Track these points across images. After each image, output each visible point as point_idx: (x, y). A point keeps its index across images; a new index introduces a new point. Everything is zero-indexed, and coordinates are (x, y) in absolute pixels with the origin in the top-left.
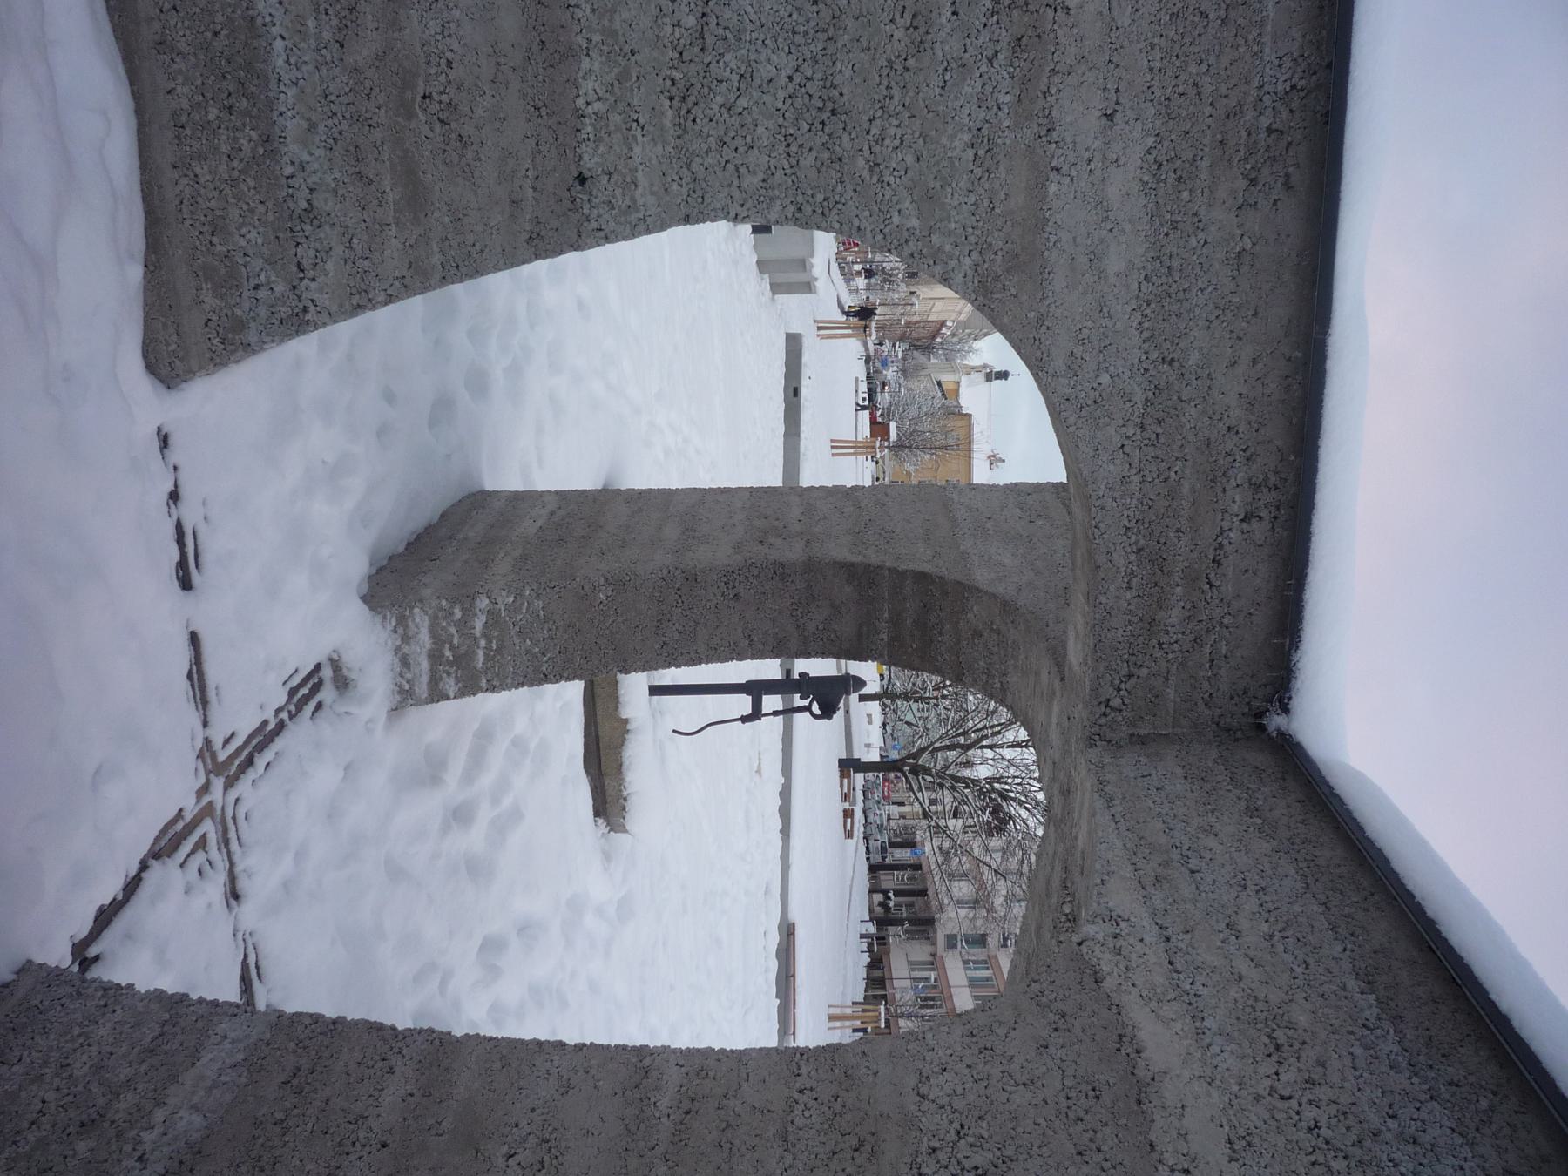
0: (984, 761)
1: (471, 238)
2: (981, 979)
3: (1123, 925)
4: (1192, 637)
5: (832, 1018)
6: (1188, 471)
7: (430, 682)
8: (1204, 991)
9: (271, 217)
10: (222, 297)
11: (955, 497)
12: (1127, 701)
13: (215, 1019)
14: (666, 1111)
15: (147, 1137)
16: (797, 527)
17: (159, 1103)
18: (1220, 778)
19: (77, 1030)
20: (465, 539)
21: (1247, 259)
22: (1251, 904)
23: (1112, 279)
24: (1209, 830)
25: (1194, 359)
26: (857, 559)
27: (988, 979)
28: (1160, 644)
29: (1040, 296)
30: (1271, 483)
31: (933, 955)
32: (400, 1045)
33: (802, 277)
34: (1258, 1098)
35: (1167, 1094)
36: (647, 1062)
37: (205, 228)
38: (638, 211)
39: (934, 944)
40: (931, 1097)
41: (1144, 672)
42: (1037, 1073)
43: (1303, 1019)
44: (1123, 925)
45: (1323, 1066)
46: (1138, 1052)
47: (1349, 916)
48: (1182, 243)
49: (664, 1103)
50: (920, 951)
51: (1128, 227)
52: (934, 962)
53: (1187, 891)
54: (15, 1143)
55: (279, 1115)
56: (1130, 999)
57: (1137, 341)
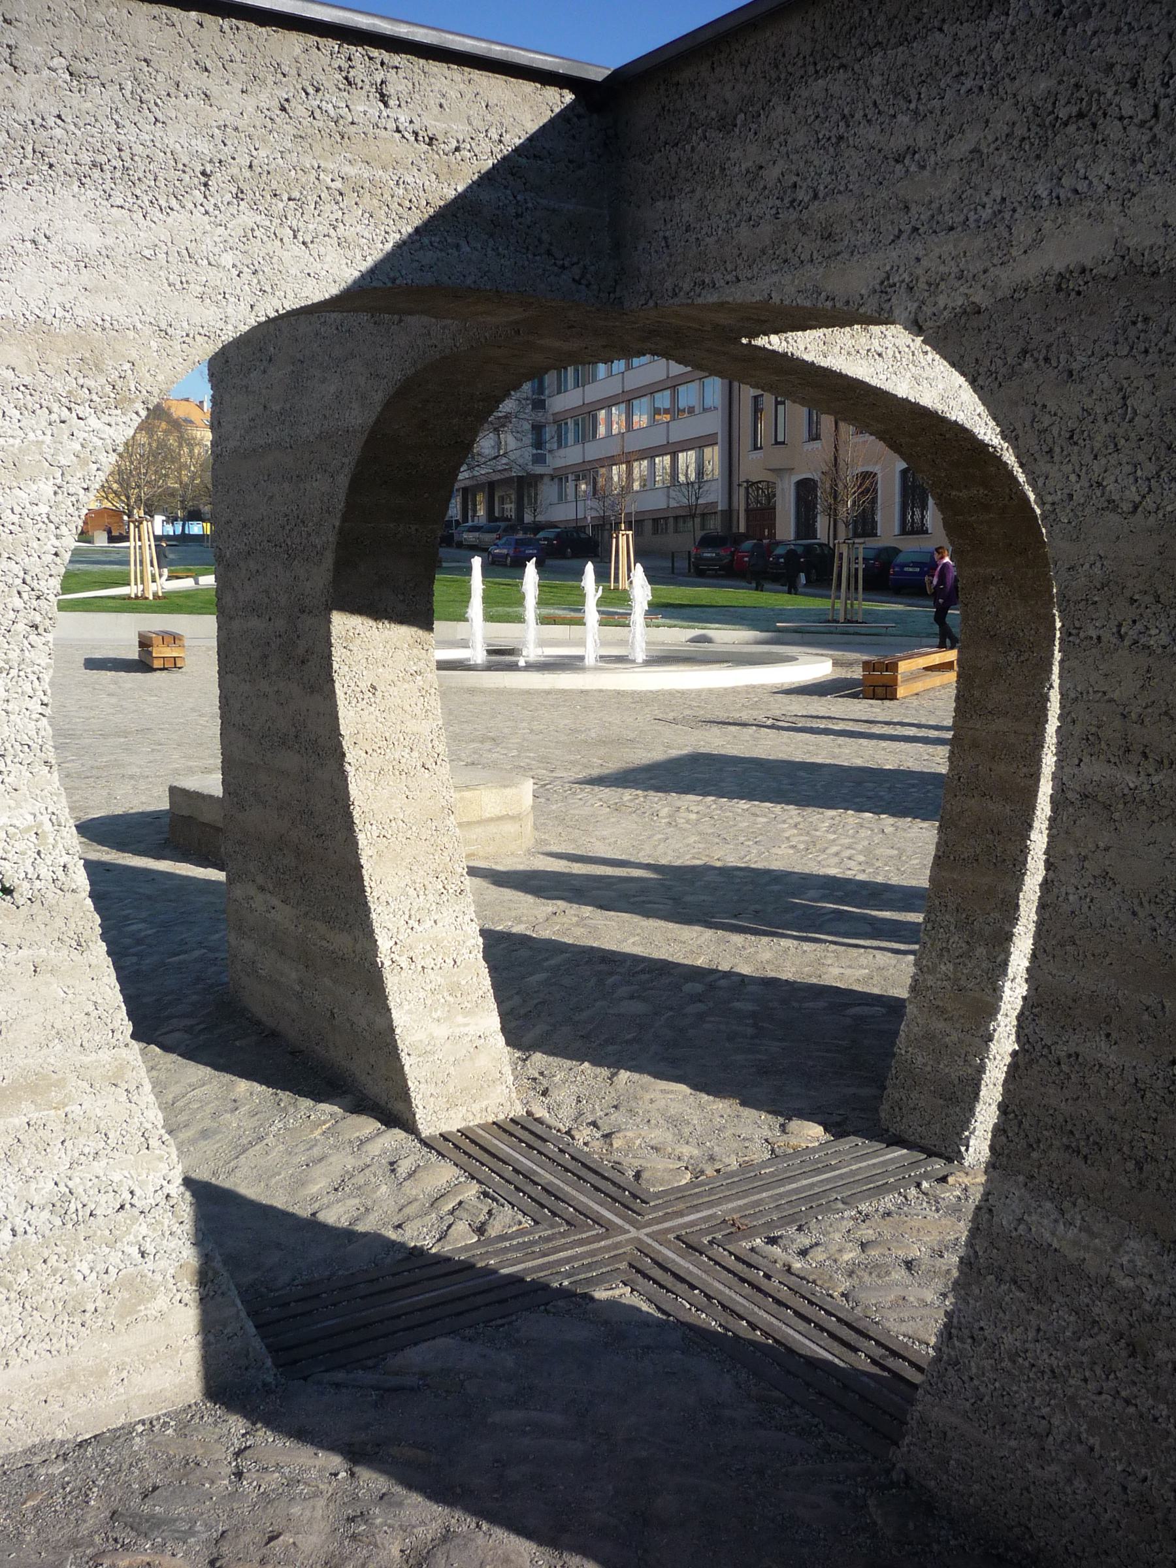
1: (80, 1017)
3: (895, 279)
4: (510, 177)
6: (331, 166)
8: (997, 193)
9: (62, 1249)
10: (154, 1292)
11: (232, 444)
12: (575, 260)
13: (995, 1230)
14: (1143, 777)
15: (1152, 1292)
16: (280, 624)
17: (1109, 1281)
18: (674, 159)
19: (1006, 1364)
20: (301, 982)
21: (77, 66)
22: (870, 134)
23: (109, 241)
24: (754, 175)
25: (203, 146)
26: (329, 559)
27: (577, 424)
28: (517, 216)
29: (131, 334)
30: (345, 65)
31: (552, 478)
32: (1038, 1047)
34: (1154, 141)
35: (1147, 243)
36: (1070, 795)
37: (78, 1320)
38: (41, 824)
39: (542, 476)
40: (1138, 499)
41: (545, 237)
42: (1108, 384)
43: (1044, 84)
44: (895, 279)
45: (1113, 65)
46: (1083, 271)
47: (890, 22)
48: (62, 147)
49: (1131, 780)
50: (548, 491)
51: (43, 216)
52: (559, 477)
53: (845, 204)
54: (1155, 1419)
55: (1130, 1165)
56: (1007, 278)
57: (183, 216)
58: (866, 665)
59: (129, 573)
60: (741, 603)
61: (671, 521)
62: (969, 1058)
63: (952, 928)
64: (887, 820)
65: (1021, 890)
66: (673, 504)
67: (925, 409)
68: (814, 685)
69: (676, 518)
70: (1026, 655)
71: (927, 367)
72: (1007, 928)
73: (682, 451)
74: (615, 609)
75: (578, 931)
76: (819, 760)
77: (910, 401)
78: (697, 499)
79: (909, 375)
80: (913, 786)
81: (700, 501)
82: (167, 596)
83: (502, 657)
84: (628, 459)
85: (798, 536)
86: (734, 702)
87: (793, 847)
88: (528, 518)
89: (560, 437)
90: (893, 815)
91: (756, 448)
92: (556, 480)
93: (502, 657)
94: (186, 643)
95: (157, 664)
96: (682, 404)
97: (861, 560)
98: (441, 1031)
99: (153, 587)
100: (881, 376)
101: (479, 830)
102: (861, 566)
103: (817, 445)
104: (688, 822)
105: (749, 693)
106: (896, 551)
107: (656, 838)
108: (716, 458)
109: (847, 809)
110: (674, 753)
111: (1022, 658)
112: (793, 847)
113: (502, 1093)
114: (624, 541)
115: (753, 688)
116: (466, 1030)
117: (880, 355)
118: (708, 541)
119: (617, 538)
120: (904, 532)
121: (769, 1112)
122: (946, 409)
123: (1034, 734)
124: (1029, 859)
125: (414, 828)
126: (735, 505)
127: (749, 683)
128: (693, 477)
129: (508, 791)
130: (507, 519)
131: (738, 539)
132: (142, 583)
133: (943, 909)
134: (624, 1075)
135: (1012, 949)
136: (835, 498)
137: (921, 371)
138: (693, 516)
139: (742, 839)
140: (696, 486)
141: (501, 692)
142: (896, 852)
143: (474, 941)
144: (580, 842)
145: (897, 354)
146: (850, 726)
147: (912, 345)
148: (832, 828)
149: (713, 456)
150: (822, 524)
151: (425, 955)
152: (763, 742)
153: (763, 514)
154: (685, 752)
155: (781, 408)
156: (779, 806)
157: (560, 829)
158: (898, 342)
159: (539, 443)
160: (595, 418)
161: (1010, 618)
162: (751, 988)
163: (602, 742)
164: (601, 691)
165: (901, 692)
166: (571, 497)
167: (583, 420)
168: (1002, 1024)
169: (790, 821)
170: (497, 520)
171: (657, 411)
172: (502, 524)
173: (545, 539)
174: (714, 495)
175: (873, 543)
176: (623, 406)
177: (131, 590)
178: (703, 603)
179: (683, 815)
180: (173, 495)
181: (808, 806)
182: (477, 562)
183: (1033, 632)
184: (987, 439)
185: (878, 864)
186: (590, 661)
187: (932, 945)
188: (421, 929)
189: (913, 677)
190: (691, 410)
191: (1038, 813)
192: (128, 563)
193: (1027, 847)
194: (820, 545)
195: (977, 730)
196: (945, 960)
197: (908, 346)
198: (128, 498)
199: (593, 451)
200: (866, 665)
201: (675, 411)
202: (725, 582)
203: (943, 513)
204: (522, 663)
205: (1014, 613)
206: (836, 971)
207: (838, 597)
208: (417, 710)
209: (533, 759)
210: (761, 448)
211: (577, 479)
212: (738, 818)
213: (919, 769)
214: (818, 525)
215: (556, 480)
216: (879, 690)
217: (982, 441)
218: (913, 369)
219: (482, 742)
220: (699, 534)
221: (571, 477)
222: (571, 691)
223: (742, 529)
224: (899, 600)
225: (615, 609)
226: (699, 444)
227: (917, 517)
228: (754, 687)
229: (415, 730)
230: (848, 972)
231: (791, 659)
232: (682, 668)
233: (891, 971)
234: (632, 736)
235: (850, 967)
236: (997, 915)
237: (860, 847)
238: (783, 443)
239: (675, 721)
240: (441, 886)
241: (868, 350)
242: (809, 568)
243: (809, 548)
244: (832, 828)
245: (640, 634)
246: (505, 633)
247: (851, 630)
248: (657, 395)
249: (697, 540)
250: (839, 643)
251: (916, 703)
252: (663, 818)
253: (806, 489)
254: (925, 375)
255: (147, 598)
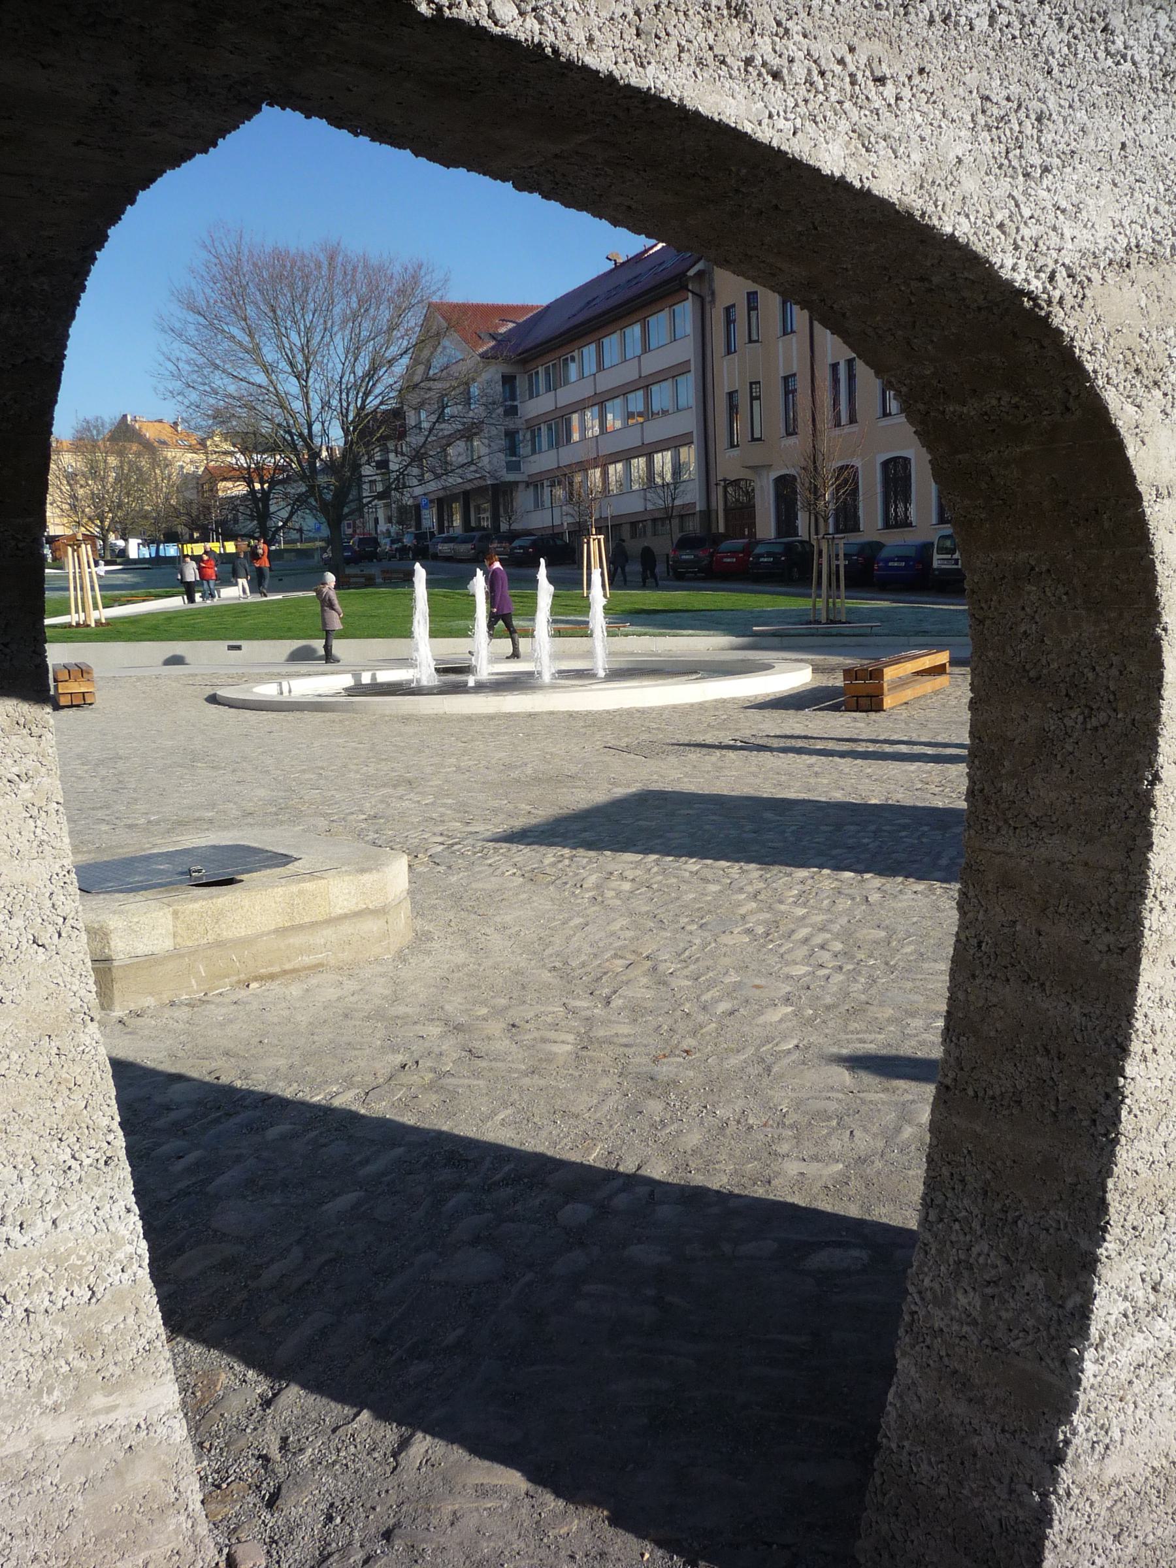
0: (325, 433)
2: (550, 436)
5: (420, 267)
7: (249, 847)
27: (550, 429)
31: (528, 485)
33: (98, 965)
39: (516, 483)
50: (523, 499)
52: (535, 483)
58: (848, 673)
59: (69, 598)
60: (719, 606)
61: (649, 523)
62: (1020, 1487)
63: (976, 1225)
64: (873, 881)
65: (1110, 1173)
66: (650, 507)
67: (883, 205)
68: (790, 696)
69: (654, 520)
70: (1102, 716)
71: (885, 113)
72: (1084, 1244)
73: (657, 452)
74: (571, 621)
75: (430, 1100)
76: (791, 795)
77: (849, 186)
78: (673, 500)
79: (844, 126)
80: (904, 827)
81: (677, 503)
82: (110, 622)
83: (454, 678)
84: (604, 463)
85: (780, 534)
86: (700, 722)
87: (749, 931)
88: (504, 527)
89: (533, 444)
90: (880, 873)
91: (732, 446)
92: (532, 488)
93: (454, 678)
94: (96, 674)
95: (63, 701)
96: (656, 407)
97: (841, 556)
98: (58, 1430)
99: (95, 615)
100: (781, 123)
101: (328, 933)
102: (842, 563)
103: (792, 440)
104: (618, 894)
105: (716, 709)
106: (880, 546)
107: (572, 924)
108: (693, 459)
109: (821, 867)
110: (620, 792)
111: (1094, 722)
112: (749, 931)
113: (177, 1531)
114: (595, 547)
115: (722, 703)
116: (108, 1419)
117: (776, 75)
118: (686, 543)
119: (588, 543)
120: (887, 525)
121: (660, 1544)
122: (930, 209)
123: (1124, 870)
124: (1124, 1113)
125: (14, 1056)
126: (713, 504)
127: (718, 697)
128: (668, 478)
129: (366, 878)
130: (484, 529)
131: (716, 539)
132: (84, 611)
133: (959, 1187)
134: (422, 1445)
135: (1096, 1288)
136: (815, 493)
137: (871, 120)
138: (670, 518)
139: (684, 920)
140: (672, 487)
141: (437, 719)
142: (883, 934)
143: (130, 1249)
144: (473, 934)
145: (816, 77)
146: (831, 745)
147: (849, 58)
148: (802, 899)
149: (689, 455)
150: (802, 521)
151: (32, 1288)
152: (727, 772)
153: (742, 513)
154: (633, 790)
155: (756, 403)
156: (737, 866)
157: (451, 915)
158: (817, 48)
159: (512, 449)
160: (569, 422)
161: (1067, 647)
162: (664, 1212)
163: (537, 780)
164: (552, 713)
165: (888, 702)
166: (547, 504)
167: (557, 424)
168: (1081, 1429)
169: (750, 889)
170: (473, 529)
171: (630, 415)
172: (477, 534)
173: (521, 547)
174: (692, 495)
175: (855, 538)
176: (596, 408)
177: (73, 618)
178: (679, 607)
179: (614, 884)
180: (145, 517)
181: (773, 863)
182: (420, 574)
183: (1114, 672)
184: (1018, 279)
185: (861, 955)
186: (547, 678)
187: (940, 1252)
188: (24, 1240)
189: (902, 683)
190: (665, 412)
191: (1138, 1025)
192: (68, 589)
193: (1118, 1090)
194: (801, 542)
195: (1011, 856)
196: (964, 1284)
197: (841, 62)
198: (102, 522)
199: (567, 456)
200: (848, 673)
201: (648, 414)
202: (702, 585)
203: (930, 449)
204: (471, 683)
205: (1075, 635)
206: (792, 1168)
207: (819, 596)
208: (21, 843)
209: (450, 807)
210: (738, 446)
211: (552, 485)
212: (684, 887)
213: (908, 802)
214: (799, 523)
215: (532, 488)
216: (862, 701)
217: (1009, 283)
218: (854, 114)
219: (395, 786)
220: (677, 535)
221: (546, 483)
222: (517, 714)
223: (722, 529)
224: (887, 597)
225: (571, 621)
226: (674, 444)
227: (901, 510)
228: (724, 701)
229: (17, 878)
230: (812, 1169)
231: (766, 667)
232: (645, 683)
233: (878, 1164)
234: (574, 769)
235: (815, 1158)
236: (1063, 1215)
237: (836, 928)
238: (760, 439)
239: (627, 750)
240: (67, 1156)
241: (748, 61)
242: (791, 568)
243: (789, 547)
244: (802, 899)
245: (601, 644)
246: (453, 648)
247: (834, 631)
248: (631, 396)
249: (675, 541)
250: (821, 646)
251: (905, 714)
252: (588, 890)
253: (785, 485)
254: (880, 129)
255: (88, 626)
